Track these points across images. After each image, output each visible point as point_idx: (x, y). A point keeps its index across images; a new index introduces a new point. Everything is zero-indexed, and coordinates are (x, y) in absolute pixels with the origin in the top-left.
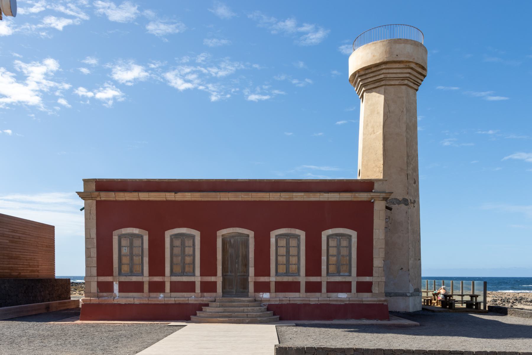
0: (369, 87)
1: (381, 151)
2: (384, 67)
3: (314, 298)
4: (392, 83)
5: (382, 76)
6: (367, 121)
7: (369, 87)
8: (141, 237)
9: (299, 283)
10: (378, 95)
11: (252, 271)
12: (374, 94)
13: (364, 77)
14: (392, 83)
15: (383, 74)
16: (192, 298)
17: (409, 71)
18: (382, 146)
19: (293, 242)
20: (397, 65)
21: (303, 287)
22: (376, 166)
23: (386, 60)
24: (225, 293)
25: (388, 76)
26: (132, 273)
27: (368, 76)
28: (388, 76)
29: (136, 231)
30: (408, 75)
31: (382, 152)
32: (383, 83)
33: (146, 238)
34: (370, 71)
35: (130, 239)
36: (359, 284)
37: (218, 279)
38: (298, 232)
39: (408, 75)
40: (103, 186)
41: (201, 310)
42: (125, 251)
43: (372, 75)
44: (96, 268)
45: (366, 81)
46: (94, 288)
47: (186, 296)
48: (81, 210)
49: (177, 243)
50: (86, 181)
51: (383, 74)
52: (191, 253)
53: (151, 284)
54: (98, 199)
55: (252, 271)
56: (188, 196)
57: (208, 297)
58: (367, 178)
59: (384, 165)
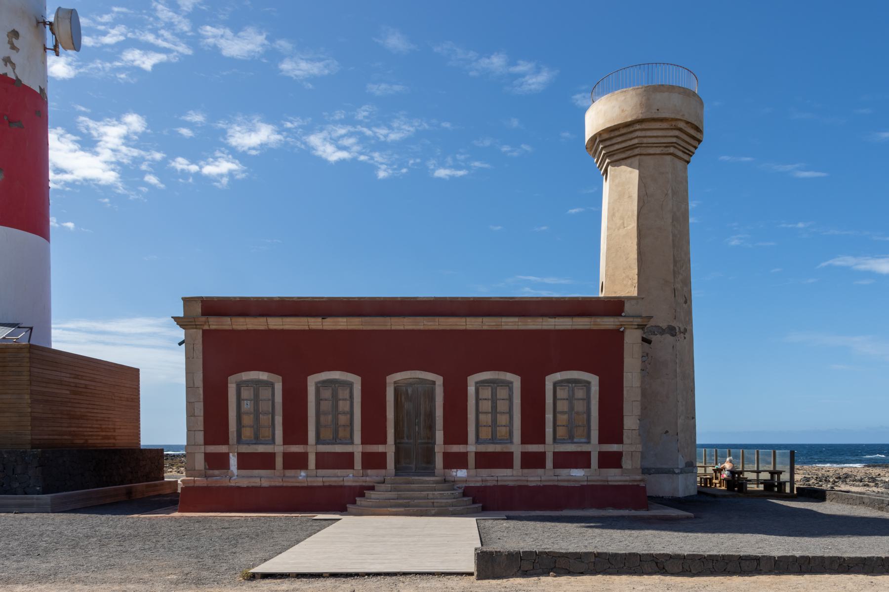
0: (615, 158)
1: (634, 255)
2: (638, 127)
3: (535, 477)
4: (651, 151)
5: (636, 141)
6: (614, 209)
7: (615, 158)
8: (271, 385)
9: (476, 453)
10: (629, 169)
11: (439, 436)
12: (623, 168)
13: (608, 143)
14: (651, 151)
15: (637, 137)
16: (349, 477)
17: (677, 133)
18: (636, 247)
19: (502, 393)
20: (658, 125)
21: (517, 460)
22: (628, 277)
23: (641, 117)
24: (399, 469)
25: (645, 140)
26: (257, 440)
27: (614, 141)
28: (645, 140)
29: (263, 376)
30: (674, 140)
31: (636, 256)
32: (637, 151)
33: (279, 387)
34: (617, 133)
35: (256, 390)
36: (602, 455)
37: (389, 449)
38: (509, 376)
39: (674, 140)
40: (213, 307)
41: (362, 495)
42: (247, 406)
43: (620, 139)
44: (202, 433)
45: (612, 149)
46: (200, 463)
47: (339, 474)
48: (180, 344)
49: (327, 393)
50: (187, 301)
51: (637, 137)
52: (347, 409)
53: (286, 455)
54: (206, 327)
55: (439, 436)
56: (342, 323)
57: (373, 475)
58: (613, 295)
59: (639, 275)
